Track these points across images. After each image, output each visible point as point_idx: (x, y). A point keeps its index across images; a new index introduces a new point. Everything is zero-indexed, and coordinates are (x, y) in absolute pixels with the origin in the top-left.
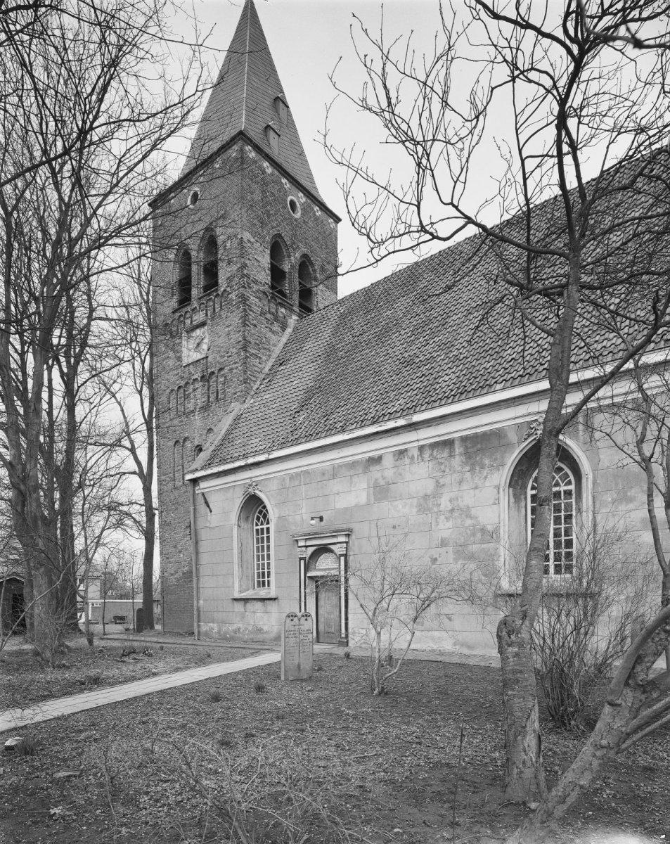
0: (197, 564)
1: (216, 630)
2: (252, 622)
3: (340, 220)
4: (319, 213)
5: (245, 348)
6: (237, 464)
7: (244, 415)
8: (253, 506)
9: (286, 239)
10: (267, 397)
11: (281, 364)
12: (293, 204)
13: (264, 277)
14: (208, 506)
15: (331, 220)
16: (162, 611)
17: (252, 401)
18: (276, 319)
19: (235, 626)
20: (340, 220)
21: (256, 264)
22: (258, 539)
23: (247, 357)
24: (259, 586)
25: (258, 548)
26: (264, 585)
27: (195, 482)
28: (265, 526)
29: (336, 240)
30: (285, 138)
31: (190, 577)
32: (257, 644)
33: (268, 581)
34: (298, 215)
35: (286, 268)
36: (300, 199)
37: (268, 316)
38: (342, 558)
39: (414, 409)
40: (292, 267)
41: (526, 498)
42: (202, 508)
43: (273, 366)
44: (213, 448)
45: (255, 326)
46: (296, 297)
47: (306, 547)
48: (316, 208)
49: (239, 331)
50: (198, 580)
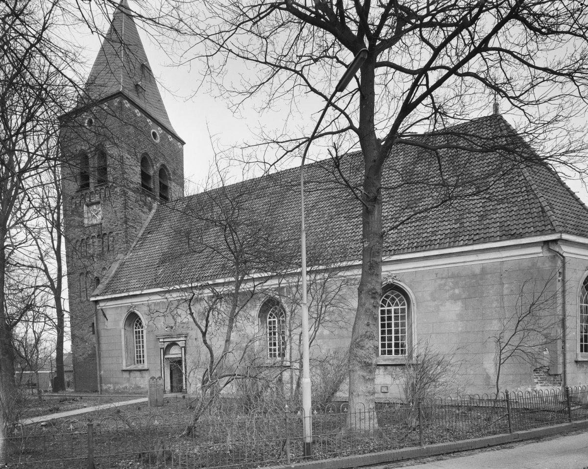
0: (99, 350)
1: (112, 388)
2: (134, 383)
3: (185, 143)
4: (171, 139)
5: (126, 222)
6: (123, 295)
7: (126, 263)
8: (133, 318)
9: (150, 155)
10: (141, 253)
11: (149, 233)
12: (154, 134)
13: (137, 179)
14: (105, 317)
15: (179, 143)
16: (80, 374)
17: (131, 255)
18: (145, 204)
19: (124, 386)
20: (185, 143)
21: (132, 171)
22: (136, 337)
23: (127, 228)
24: (271, 356)
25: (137, 341)
26: (141, 362)
27: (96, 302)
28: (140, 330)
29: (183, 155)
30: (148, 91)
31: (94, 357)
32: (137, 392)
33: (143, 360)
34: (158, 141)
35: (151, 173)
36: (159, 131)
37: (140, 203)
38: (183, 349)
39: (217, 276)
40: (155, 173)
41: (266, 323)
42: (101, 317)
43: (144, 233)
44: (107, 282)
45: (132, 209)
46: (157, 190)
47: (164, 342)
48: (169, 136)
49: (122, 212)
50: (100, 359)
